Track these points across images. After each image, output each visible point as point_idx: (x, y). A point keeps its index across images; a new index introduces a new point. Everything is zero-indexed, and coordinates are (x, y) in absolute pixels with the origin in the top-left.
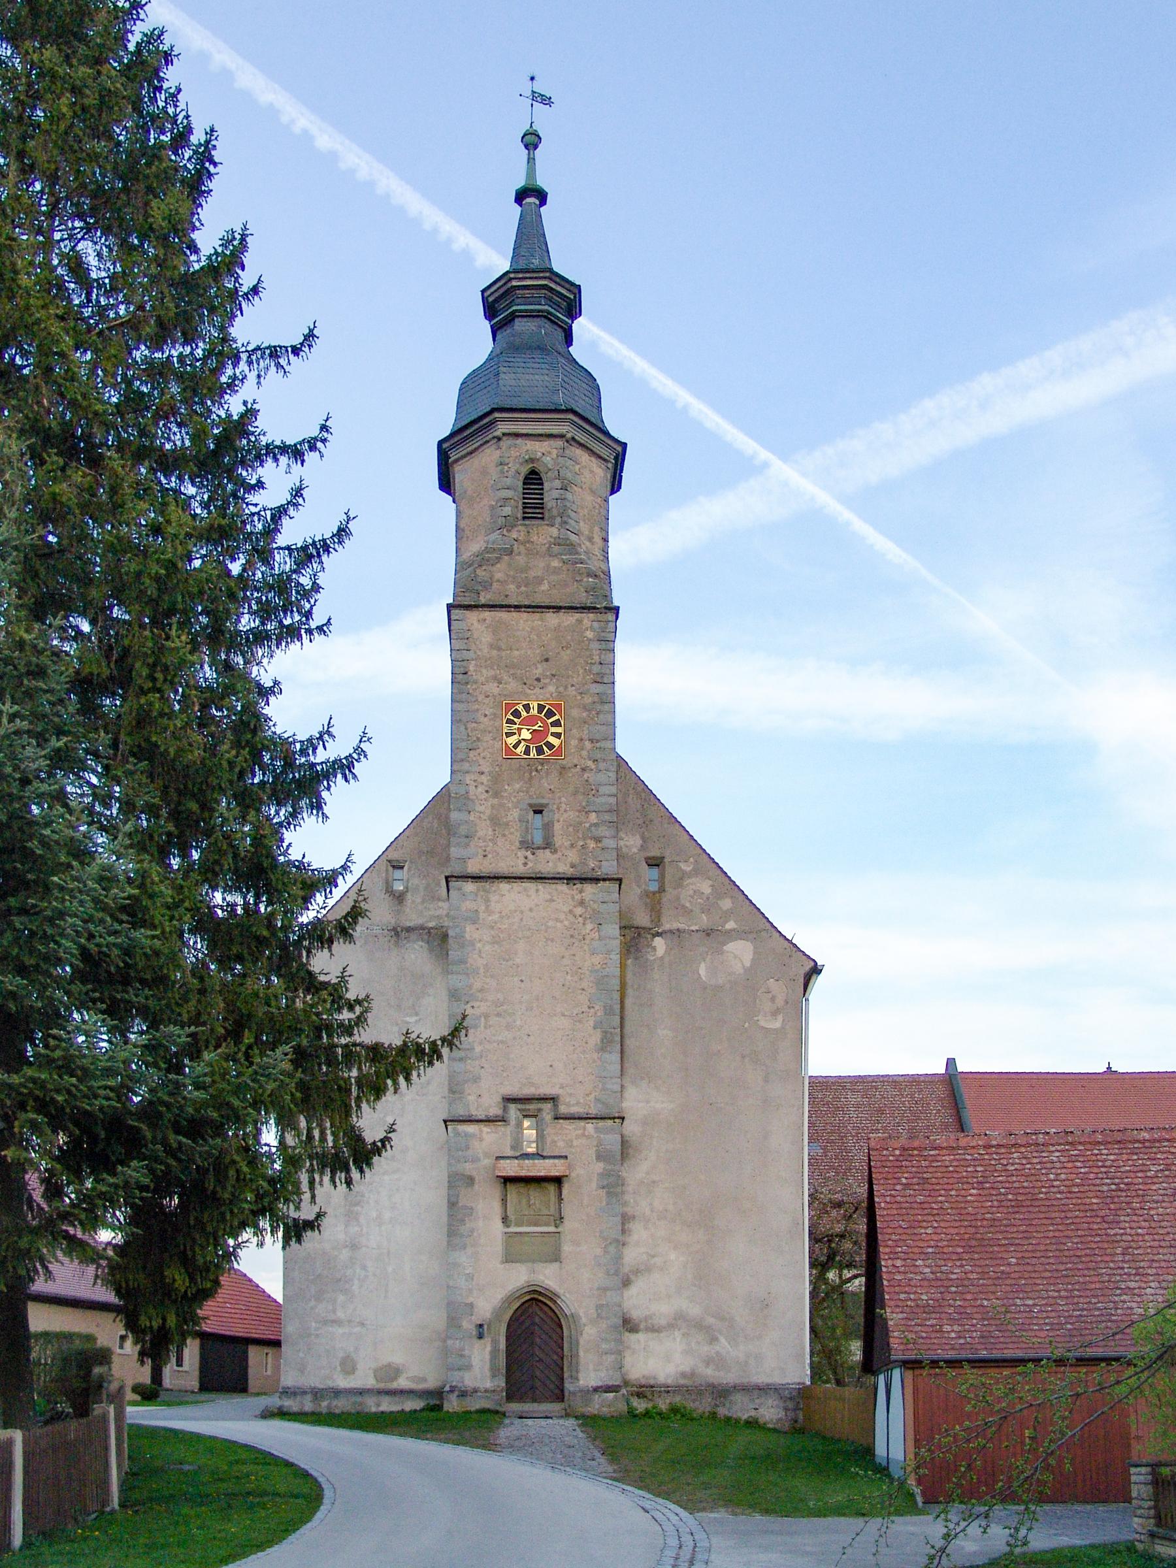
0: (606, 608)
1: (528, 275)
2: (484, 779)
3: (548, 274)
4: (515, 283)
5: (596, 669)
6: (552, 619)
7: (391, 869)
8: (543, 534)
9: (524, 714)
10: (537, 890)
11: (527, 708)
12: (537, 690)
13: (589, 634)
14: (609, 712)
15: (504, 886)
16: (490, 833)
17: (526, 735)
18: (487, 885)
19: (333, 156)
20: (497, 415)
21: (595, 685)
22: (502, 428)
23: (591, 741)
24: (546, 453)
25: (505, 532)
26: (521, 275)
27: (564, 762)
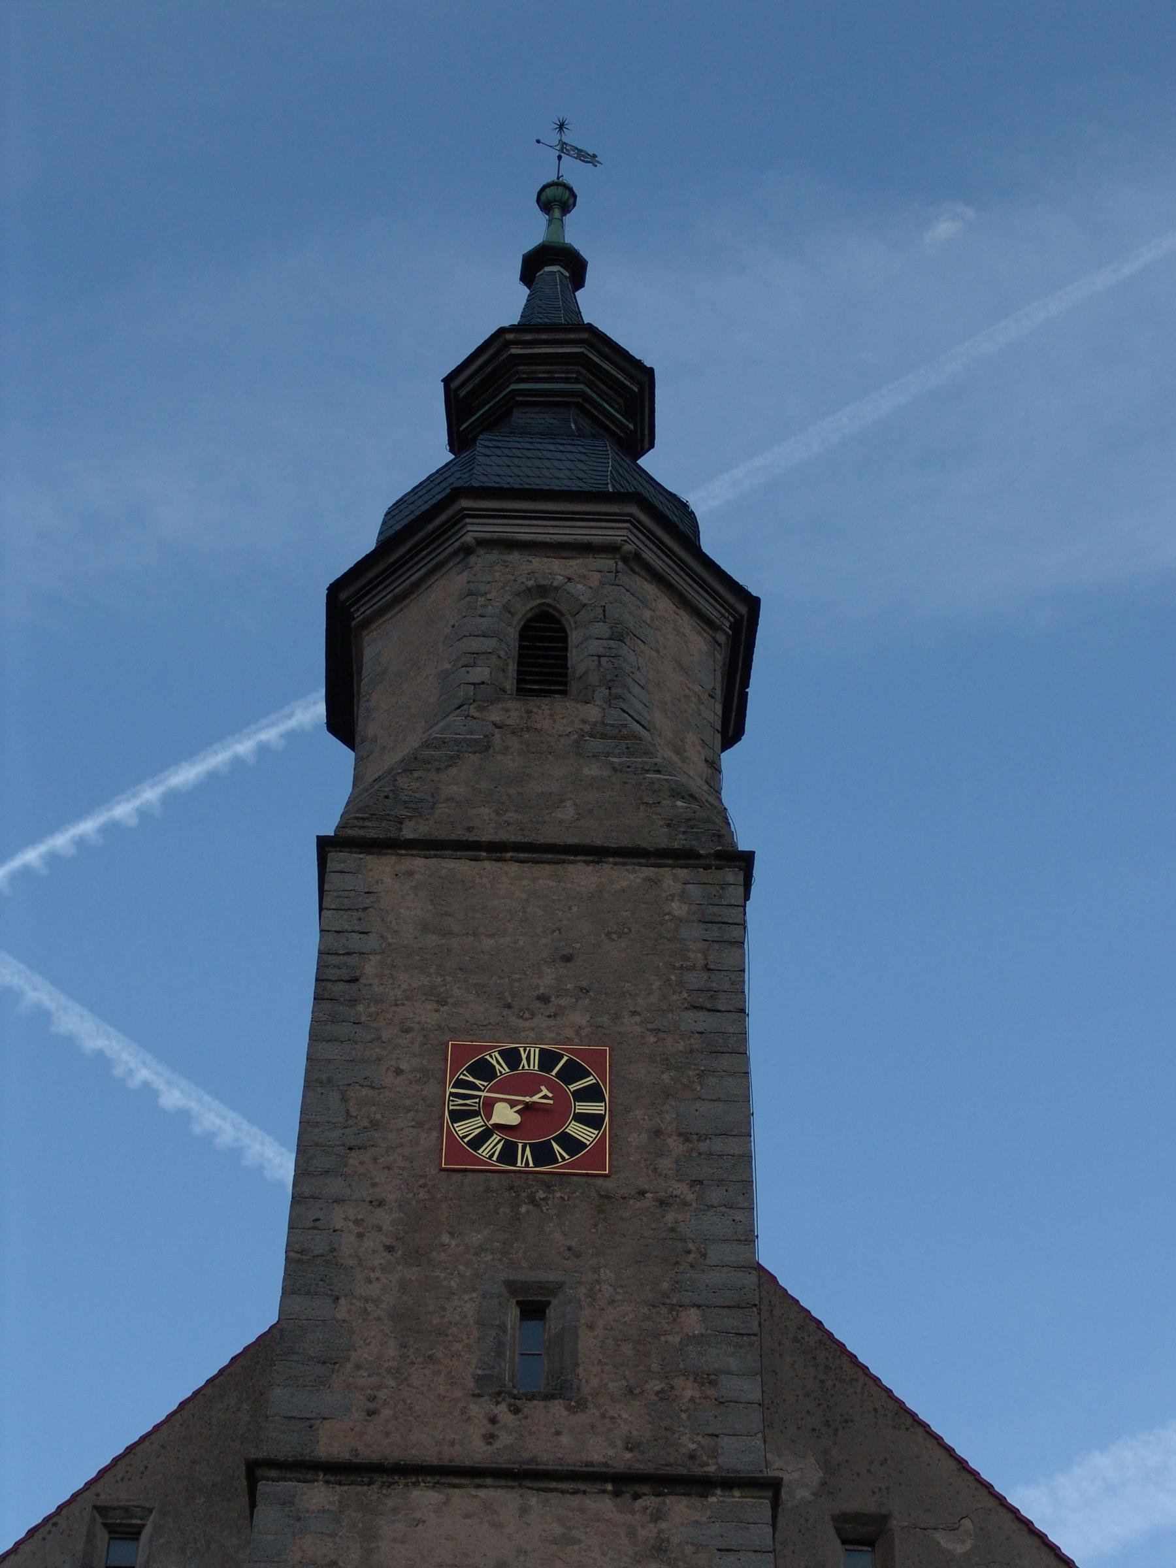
0: (719, 855)
1: (543, 337)
2: (384, 1218)
3: (585, 336)
4: (515, 351)
5: (695, 980)
6: (583, 876)
7: (102, 1536)
8: (558, 718)
9: (502, 1069)
10: (524, 1510)
11: (512, 1057)
12: (541, 1022)
13: (677, 908)
14: (733, 1074)
15: (424, 1497)
16: (392, 1351)
17: (505, 1114)
18: (372, 1493)
19: (184, 1116)
20: (465, 503)
21: (690, 1015)
22: (474, 530)
23: (686, 1137)
24: (578, 580)
25: (473, 711)
26: (529, 337)
27: (609, 1184)
